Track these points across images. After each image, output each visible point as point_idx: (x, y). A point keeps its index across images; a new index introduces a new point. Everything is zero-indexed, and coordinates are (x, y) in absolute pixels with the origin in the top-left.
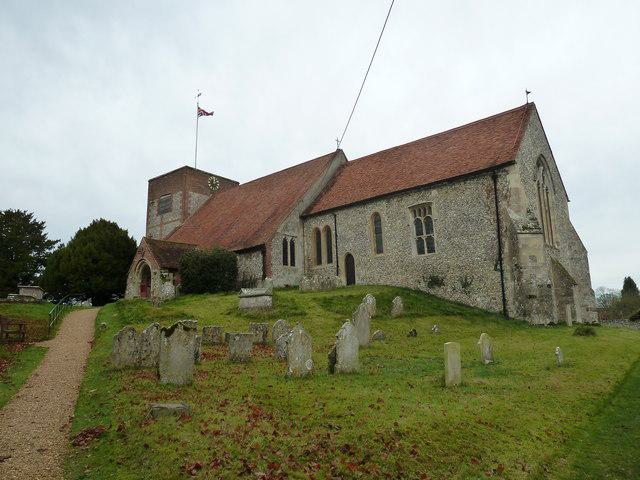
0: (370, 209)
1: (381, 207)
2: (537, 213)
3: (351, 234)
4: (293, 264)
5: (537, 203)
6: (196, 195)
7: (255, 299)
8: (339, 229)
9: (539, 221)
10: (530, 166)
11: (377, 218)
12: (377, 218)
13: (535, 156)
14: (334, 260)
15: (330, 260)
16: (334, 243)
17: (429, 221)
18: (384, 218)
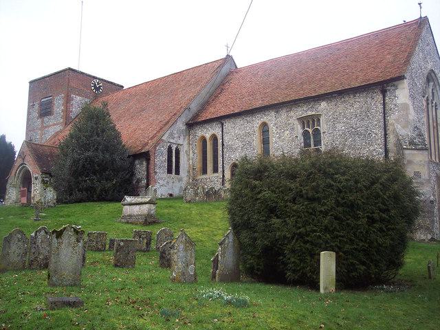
0: (257, 121)
1: (270, 118)
2: (424, 129)
3: (238, 144)
4: (177, 172)
5: (425, 120)
6: (78, 98)
7: (138, 207)
8: (226, 138)
9: (426, 136)
10: (420, 83)
11: (264, 129)
12: (264, 126)
13: (426, 72)
14: (220, 169)
15: (215, 170)
16: (220, 153)
17: (317, 133)
18: (272, 129)
